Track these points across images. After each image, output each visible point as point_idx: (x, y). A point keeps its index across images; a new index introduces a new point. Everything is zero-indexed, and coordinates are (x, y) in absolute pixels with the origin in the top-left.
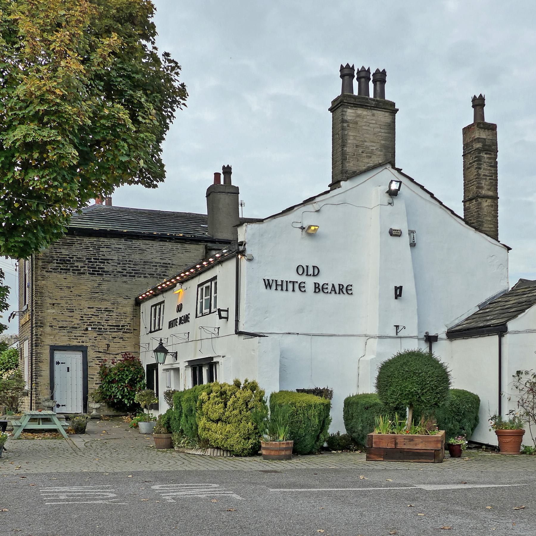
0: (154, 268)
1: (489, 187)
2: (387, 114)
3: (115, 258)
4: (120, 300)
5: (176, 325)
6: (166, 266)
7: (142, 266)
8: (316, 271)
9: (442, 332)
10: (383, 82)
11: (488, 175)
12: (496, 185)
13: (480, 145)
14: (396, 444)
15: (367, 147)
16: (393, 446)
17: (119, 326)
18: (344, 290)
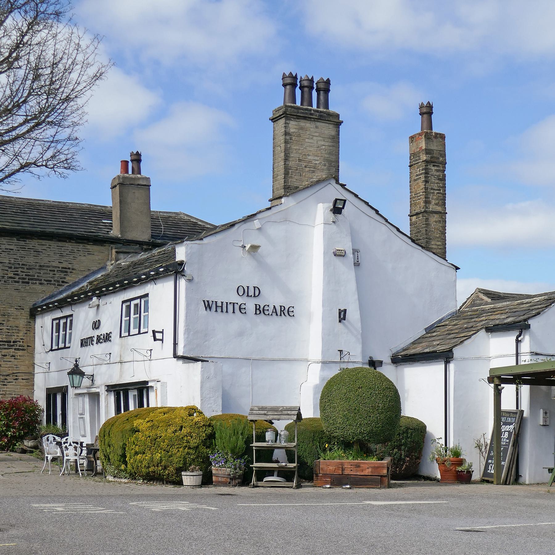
0: (52, 273)
1: (437, 201)
2: (331, 126)
4: (12, 311)
5: (92, 344)
6: (65, 271)
7: (38, 271)
8: (257, 292)
9: (386, 358)
11: (436, 188)
12: (444, 199)
13: (431, 161)
14: (343, 470)
15: (310, 162)
16: (340, 472)
17: (10, 342)
18: (285, 312)
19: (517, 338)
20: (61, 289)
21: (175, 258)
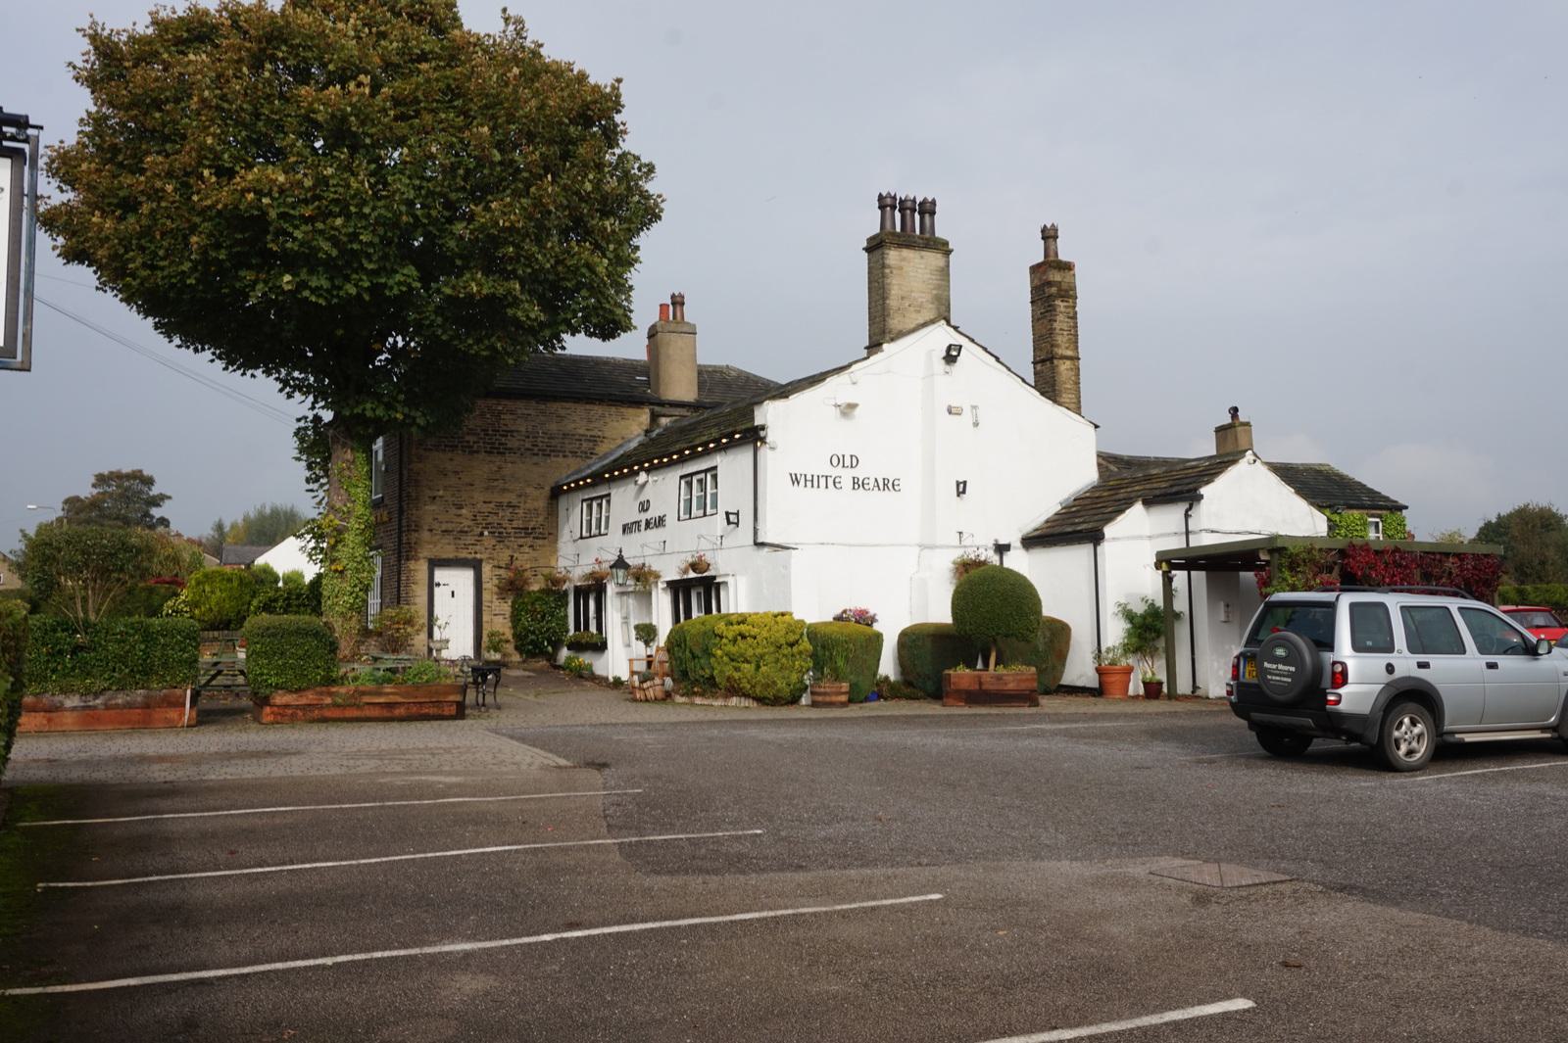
2: (939, 256)
3: (523, 429)
4: (529, 490)
8: (855, 462)
10: (933, 213)
13: (1051, 287)
16: (977, 687)
18: (887, 485)
19: (1187, 511)
20: (589, 462)
21: (753, 419)
